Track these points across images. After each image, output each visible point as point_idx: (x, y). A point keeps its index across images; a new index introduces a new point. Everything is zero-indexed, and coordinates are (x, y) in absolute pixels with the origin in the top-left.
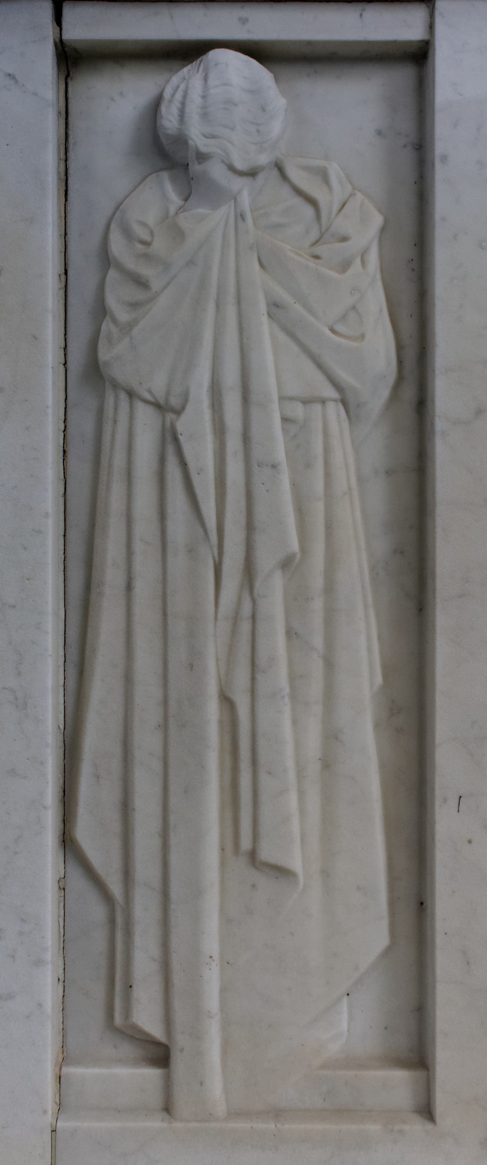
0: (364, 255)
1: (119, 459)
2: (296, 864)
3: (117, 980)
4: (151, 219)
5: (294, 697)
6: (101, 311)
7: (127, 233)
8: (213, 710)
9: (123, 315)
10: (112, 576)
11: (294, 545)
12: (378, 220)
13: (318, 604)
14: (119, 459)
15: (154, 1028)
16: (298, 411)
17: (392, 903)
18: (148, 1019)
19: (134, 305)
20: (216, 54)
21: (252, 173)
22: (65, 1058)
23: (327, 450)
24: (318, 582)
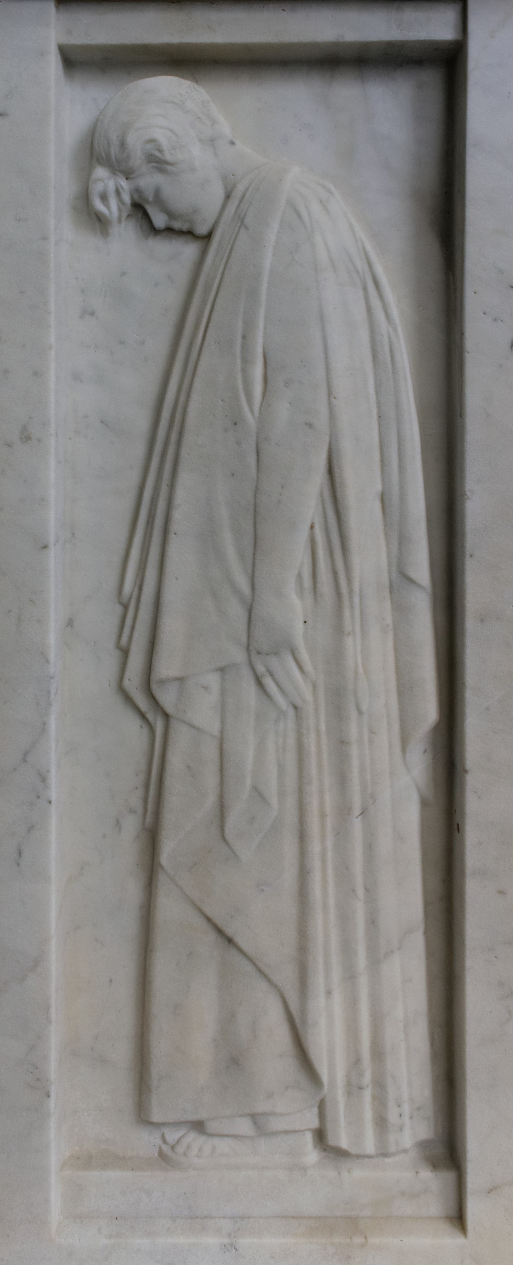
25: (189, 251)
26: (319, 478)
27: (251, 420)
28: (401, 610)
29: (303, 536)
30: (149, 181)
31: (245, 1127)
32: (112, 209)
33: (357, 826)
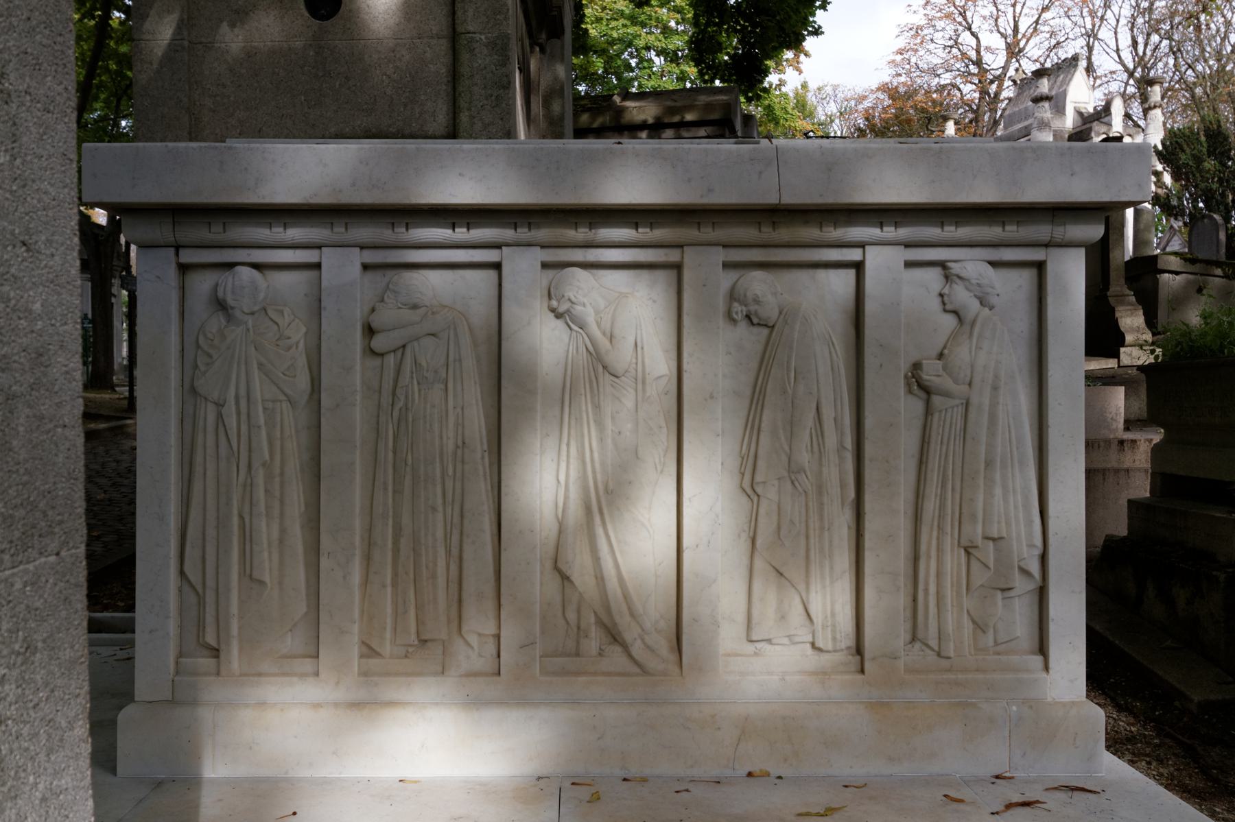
0: (297, 343)
1: (201, 423)
2: (267, 579)
3: (201, 625)
4: (214, 331)
5: (267, 515)
6: (196, 367)
7: (205, 335)
8: (235, 520)
9: (202, 368)
10: (198, 469)
11: (267, 457)
12: (304, 330)
13: (277, 479)
14: (201, 423)
15: (213, 643)
16: (270, 405)
17: (307, 595)
18: (211, 639)
19: (208, 364)
20: (239, 268)
21: (253, 314)
22: (180, 655)
23: (282, 420)
24: (277, 471)
25: (765, 331)
26: (814, 410)
27: (790, 391)
28: (841, 459)
29: (808, 431)
30: (753, 308)
31: (786, 641)
32: (739, 317)
33: (826, 534)
